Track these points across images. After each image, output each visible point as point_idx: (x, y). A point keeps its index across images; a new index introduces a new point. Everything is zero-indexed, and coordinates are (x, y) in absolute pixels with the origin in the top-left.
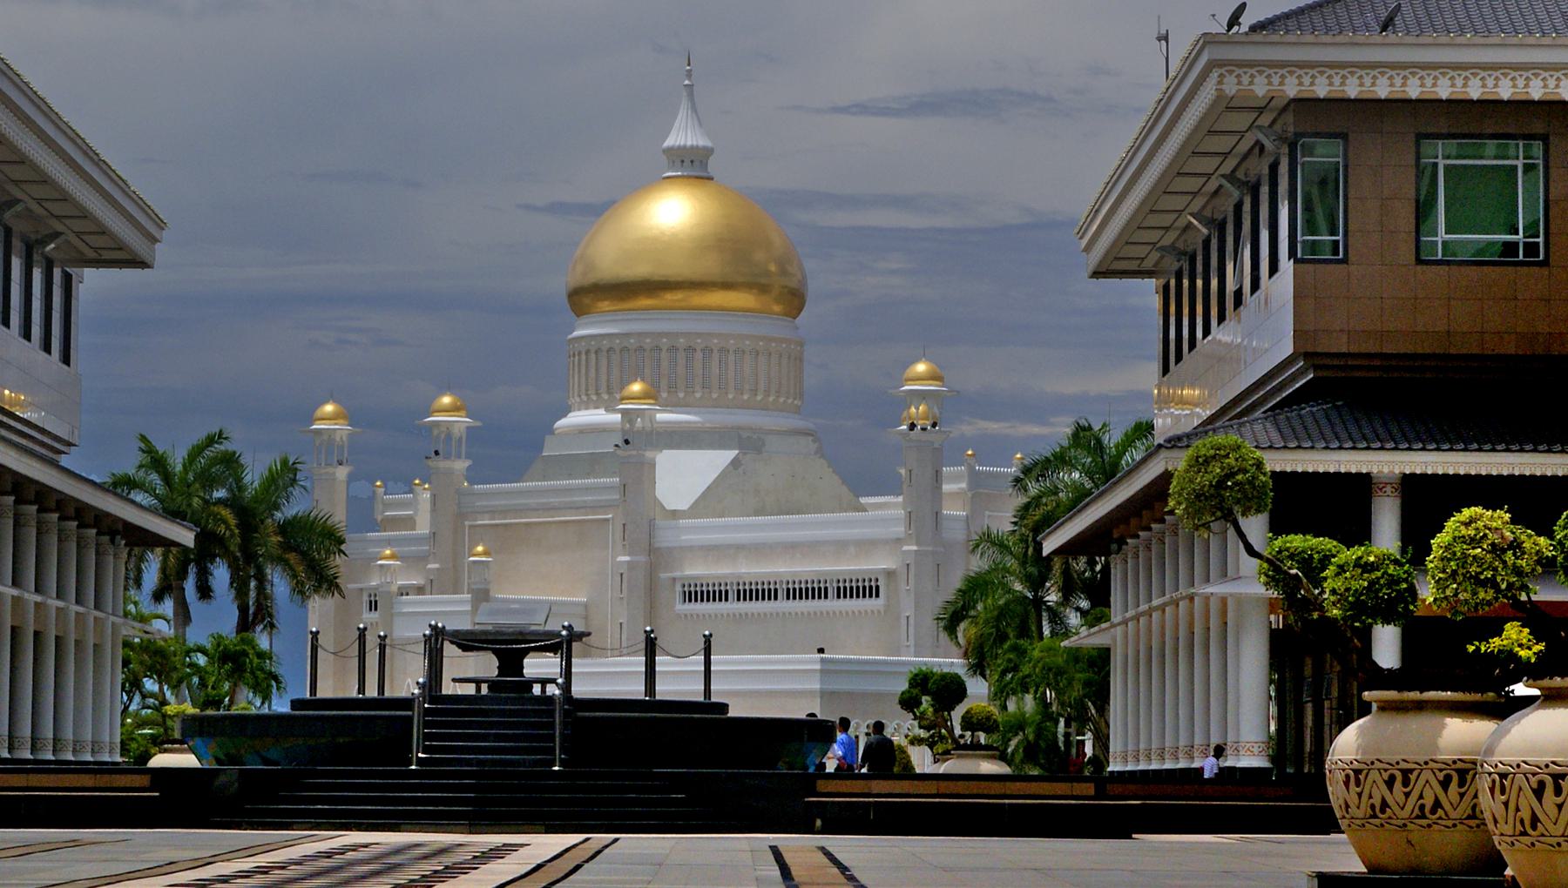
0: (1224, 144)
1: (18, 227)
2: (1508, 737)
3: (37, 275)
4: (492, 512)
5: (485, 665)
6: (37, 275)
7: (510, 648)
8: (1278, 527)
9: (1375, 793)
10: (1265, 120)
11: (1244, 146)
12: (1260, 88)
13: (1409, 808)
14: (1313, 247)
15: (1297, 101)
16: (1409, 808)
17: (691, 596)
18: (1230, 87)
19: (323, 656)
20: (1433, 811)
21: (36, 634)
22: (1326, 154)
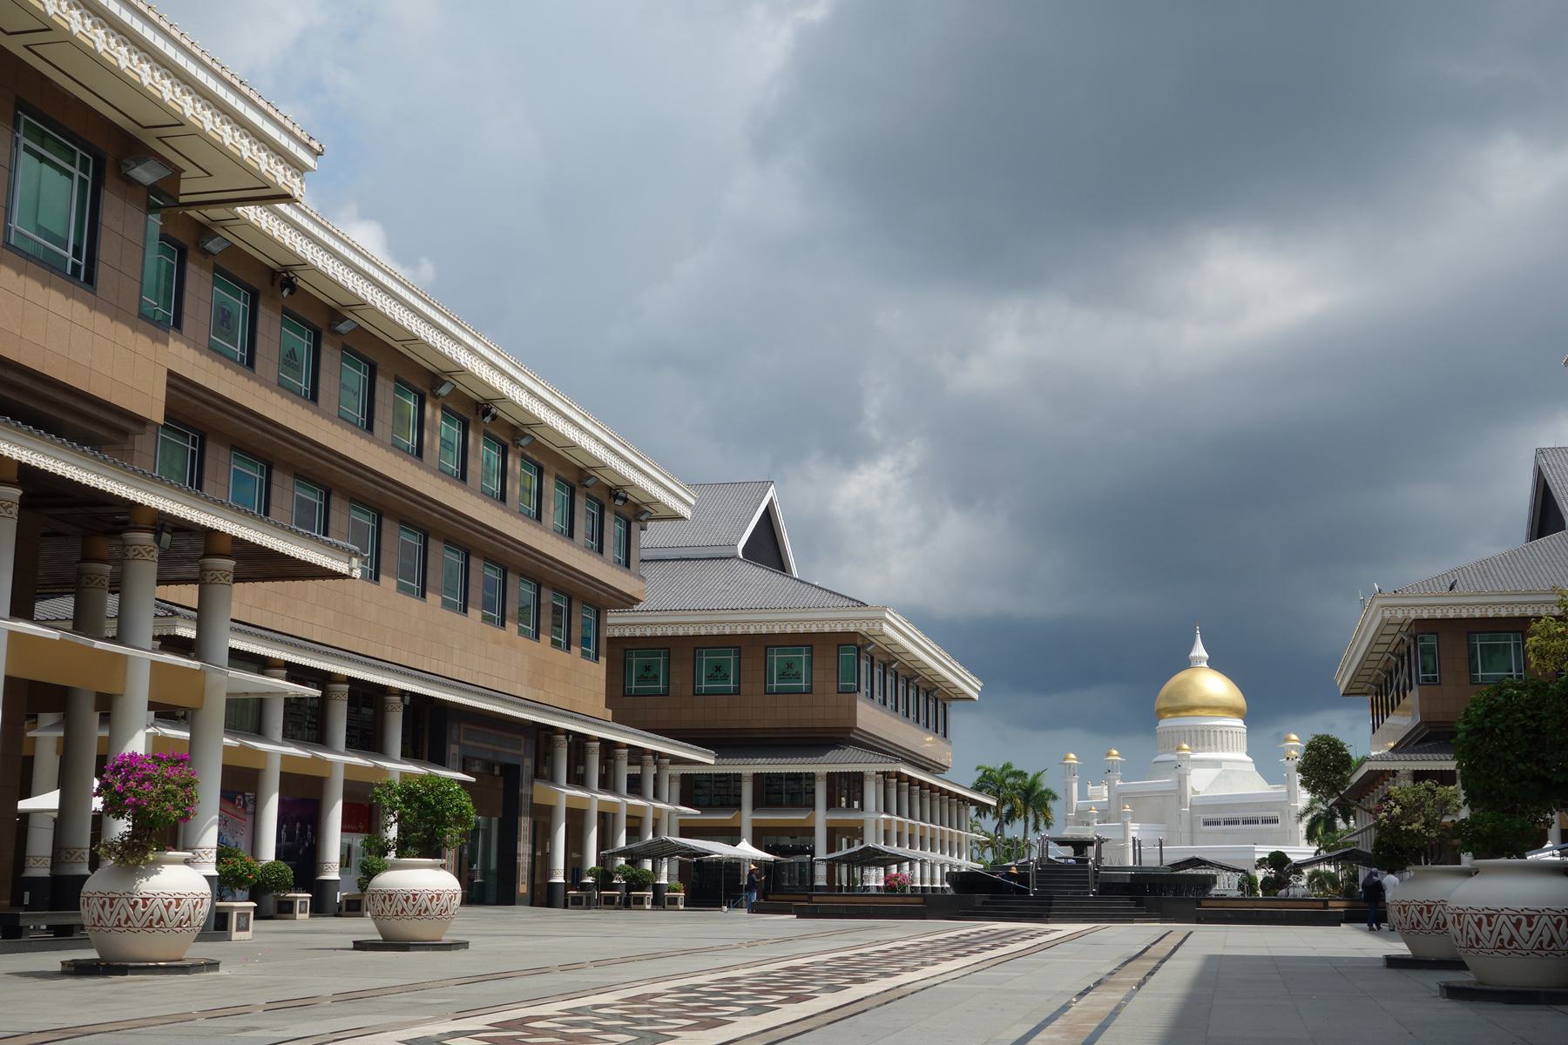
0: (1388, 639)
1: (922, 686)
2: (154, 879)
3: (931, 704)
4: (656, 778)
5: (1068, 851)
6: (931, 704)
7: (1080, 846)
8: (552, 779)
9: (1504, 930)
10: (1404, 628)
11: (1397, 640)
12: (1400, 615)
13: (1531, 943)
14: (1426, 679)
15: (1416, 621)
16: (1531, 943)
17: (1207, 823)
18: (1387, 615)
19: (1041, 844)
20: (1510, 943)
21: (899, 834)
22: (1431, 641)
